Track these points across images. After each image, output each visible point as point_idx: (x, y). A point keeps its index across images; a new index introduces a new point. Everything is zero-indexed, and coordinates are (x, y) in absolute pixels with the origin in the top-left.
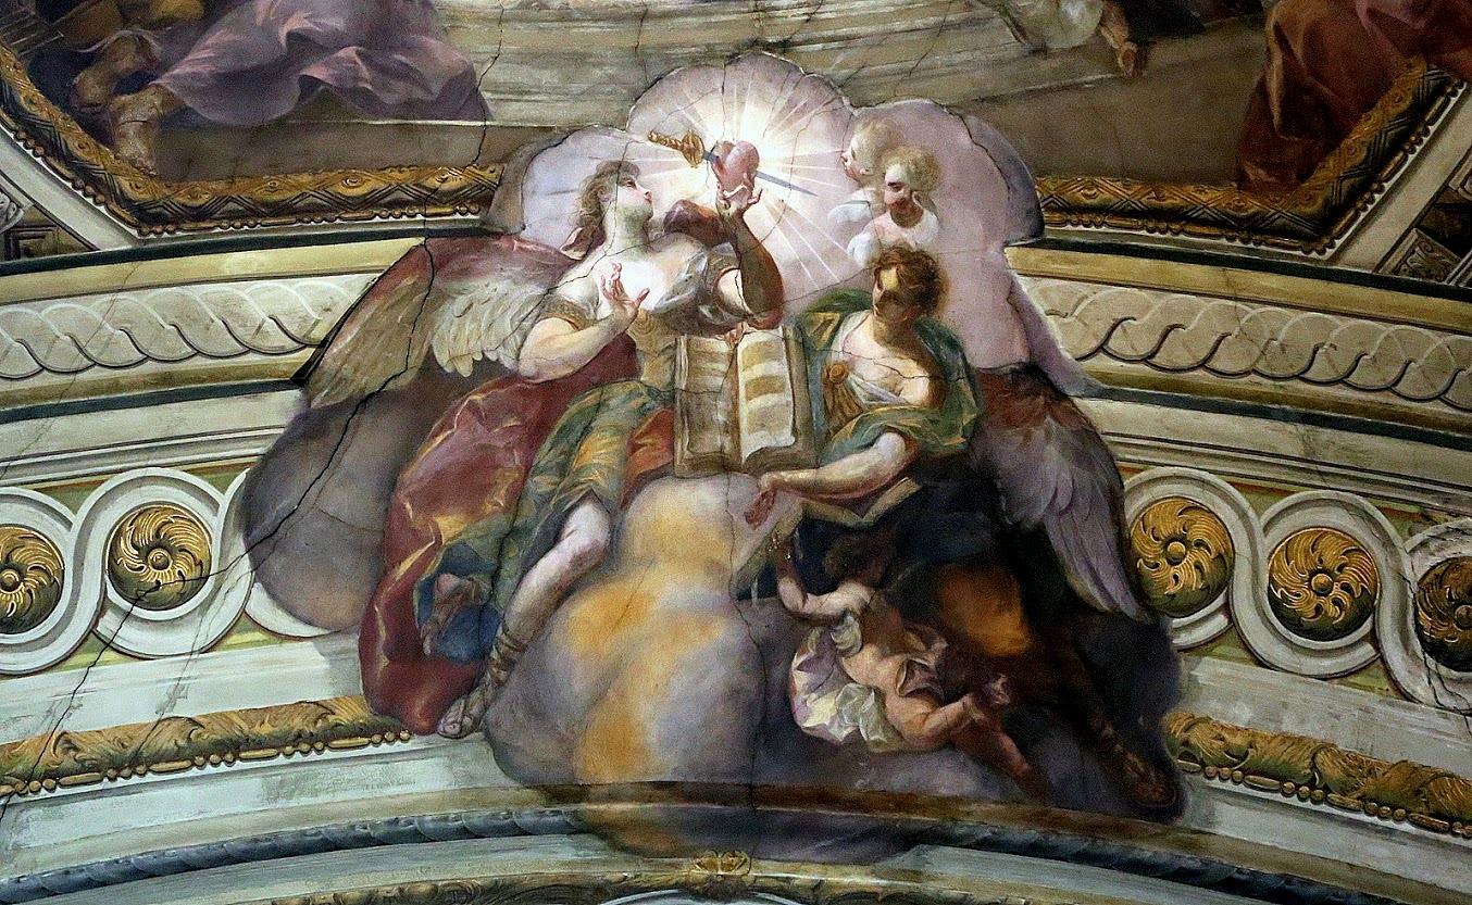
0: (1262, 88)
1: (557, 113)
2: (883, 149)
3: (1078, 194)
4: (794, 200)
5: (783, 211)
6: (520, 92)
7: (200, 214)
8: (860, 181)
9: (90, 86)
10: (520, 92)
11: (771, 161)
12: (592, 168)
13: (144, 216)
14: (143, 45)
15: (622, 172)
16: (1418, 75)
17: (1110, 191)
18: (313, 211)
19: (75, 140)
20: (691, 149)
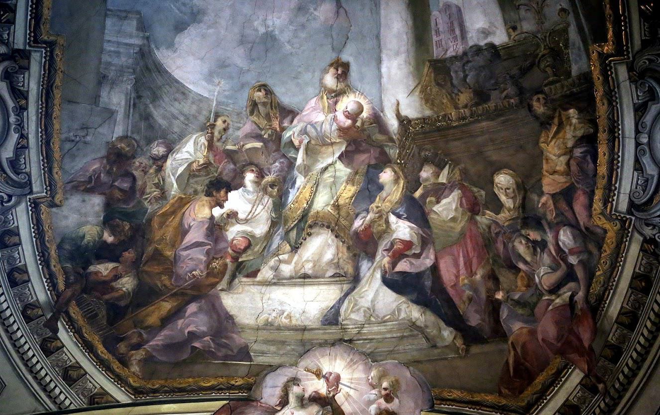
0: (507, 362)
1: (275, 360)
2: (381, 378)
3: (446, 395)
4: (352, 392)
5: (348, 396)
6: (263, 353)
7: (155, 391)
8: (373, 387)
9: (122, 347)
10: (263, 353)
11: (345, 378)
12: (285, 379)
13: (137, 391)
14: (140, 335)
15: (295, 381)
16: (558, 362)
17: (456, 394)
18: (192, 391)
19: (116, 365)
20: (318, 374)
